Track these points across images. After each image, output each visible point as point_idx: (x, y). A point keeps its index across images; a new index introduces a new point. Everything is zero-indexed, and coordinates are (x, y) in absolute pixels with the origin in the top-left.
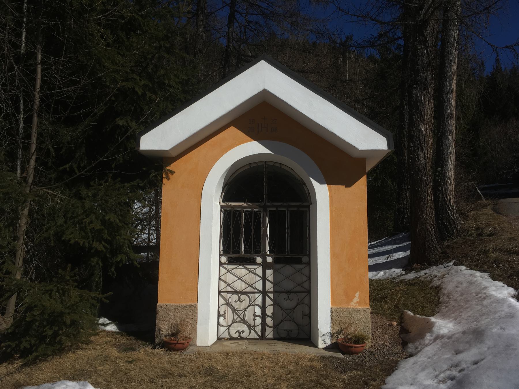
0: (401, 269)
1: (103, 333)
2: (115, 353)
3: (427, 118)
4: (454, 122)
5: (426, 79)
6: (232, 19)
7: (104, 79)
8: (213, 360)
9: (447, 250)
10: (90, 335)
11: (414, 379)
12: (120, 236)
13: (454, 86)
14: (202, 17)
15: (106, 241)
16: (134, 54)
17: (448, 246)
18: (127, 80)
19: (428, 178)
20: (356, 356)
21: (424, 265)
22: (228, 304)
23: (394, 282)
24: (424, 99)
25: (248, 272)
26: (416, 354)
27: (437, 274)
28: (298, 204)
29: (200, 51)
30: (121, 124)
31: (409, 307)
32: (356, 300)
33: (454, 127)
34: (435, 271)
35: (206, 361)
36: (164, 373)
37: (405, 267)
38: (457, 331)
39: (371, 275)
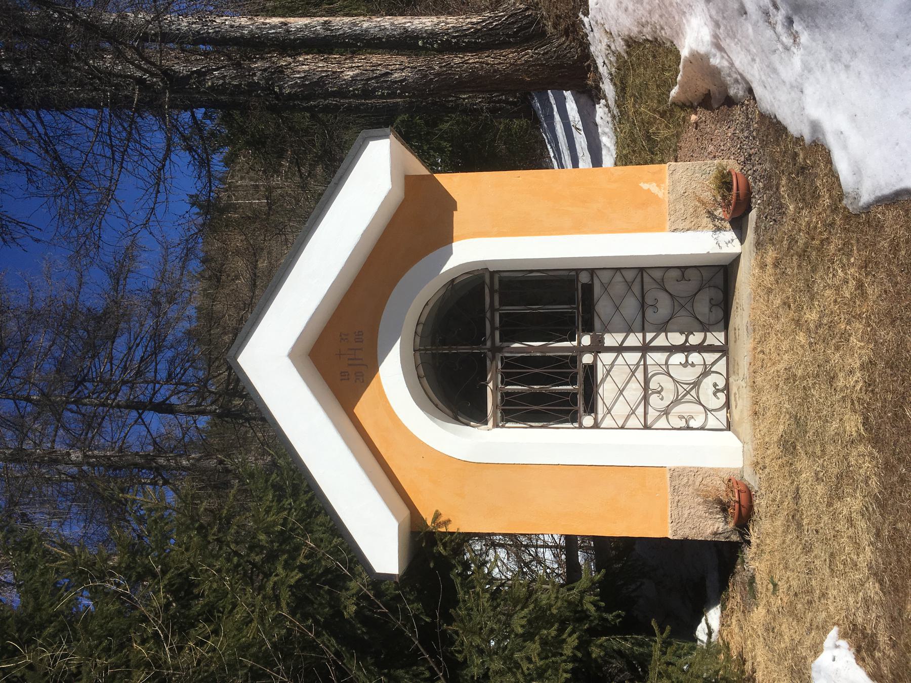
0: (597, 106)
1: (725, 634)
2: (759, 614)
3: (334, 67)
4: (338, 19)
5: (265, 70)
6: (165, 408)
7: (276, 639)
8: (767, 439)
9: (562, 27)
10: (728, 657)
11: (792, 87)
12: (551, 606)
13: (276, 20)
14: (161, 461)
15: (561, 631)
16: (231, 585)
17: (555, 26)
18: (277, 598)
19: (436, 64)
20: (753, 187)
21: (589, 66)
22: (666, 412)
23: (620, 119)
24: (299, 72)
25: (609, 378)
26: (747, 83)
27: (604, 44)
28: (487, 291)
29: (221, 462)
30: (354, 608)
31: (663, 94)
32: (653, 188)
33: (347, 19)
34: (599, 48)
35: (769, 452)
36: (793, 526)
37: (593, 101)
38: (706, 10)
39: (608, 159)
